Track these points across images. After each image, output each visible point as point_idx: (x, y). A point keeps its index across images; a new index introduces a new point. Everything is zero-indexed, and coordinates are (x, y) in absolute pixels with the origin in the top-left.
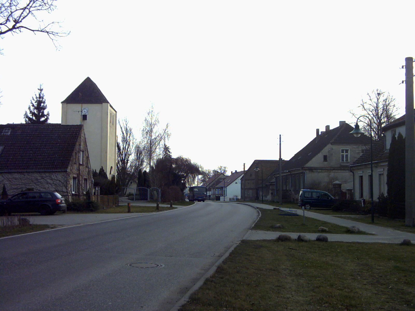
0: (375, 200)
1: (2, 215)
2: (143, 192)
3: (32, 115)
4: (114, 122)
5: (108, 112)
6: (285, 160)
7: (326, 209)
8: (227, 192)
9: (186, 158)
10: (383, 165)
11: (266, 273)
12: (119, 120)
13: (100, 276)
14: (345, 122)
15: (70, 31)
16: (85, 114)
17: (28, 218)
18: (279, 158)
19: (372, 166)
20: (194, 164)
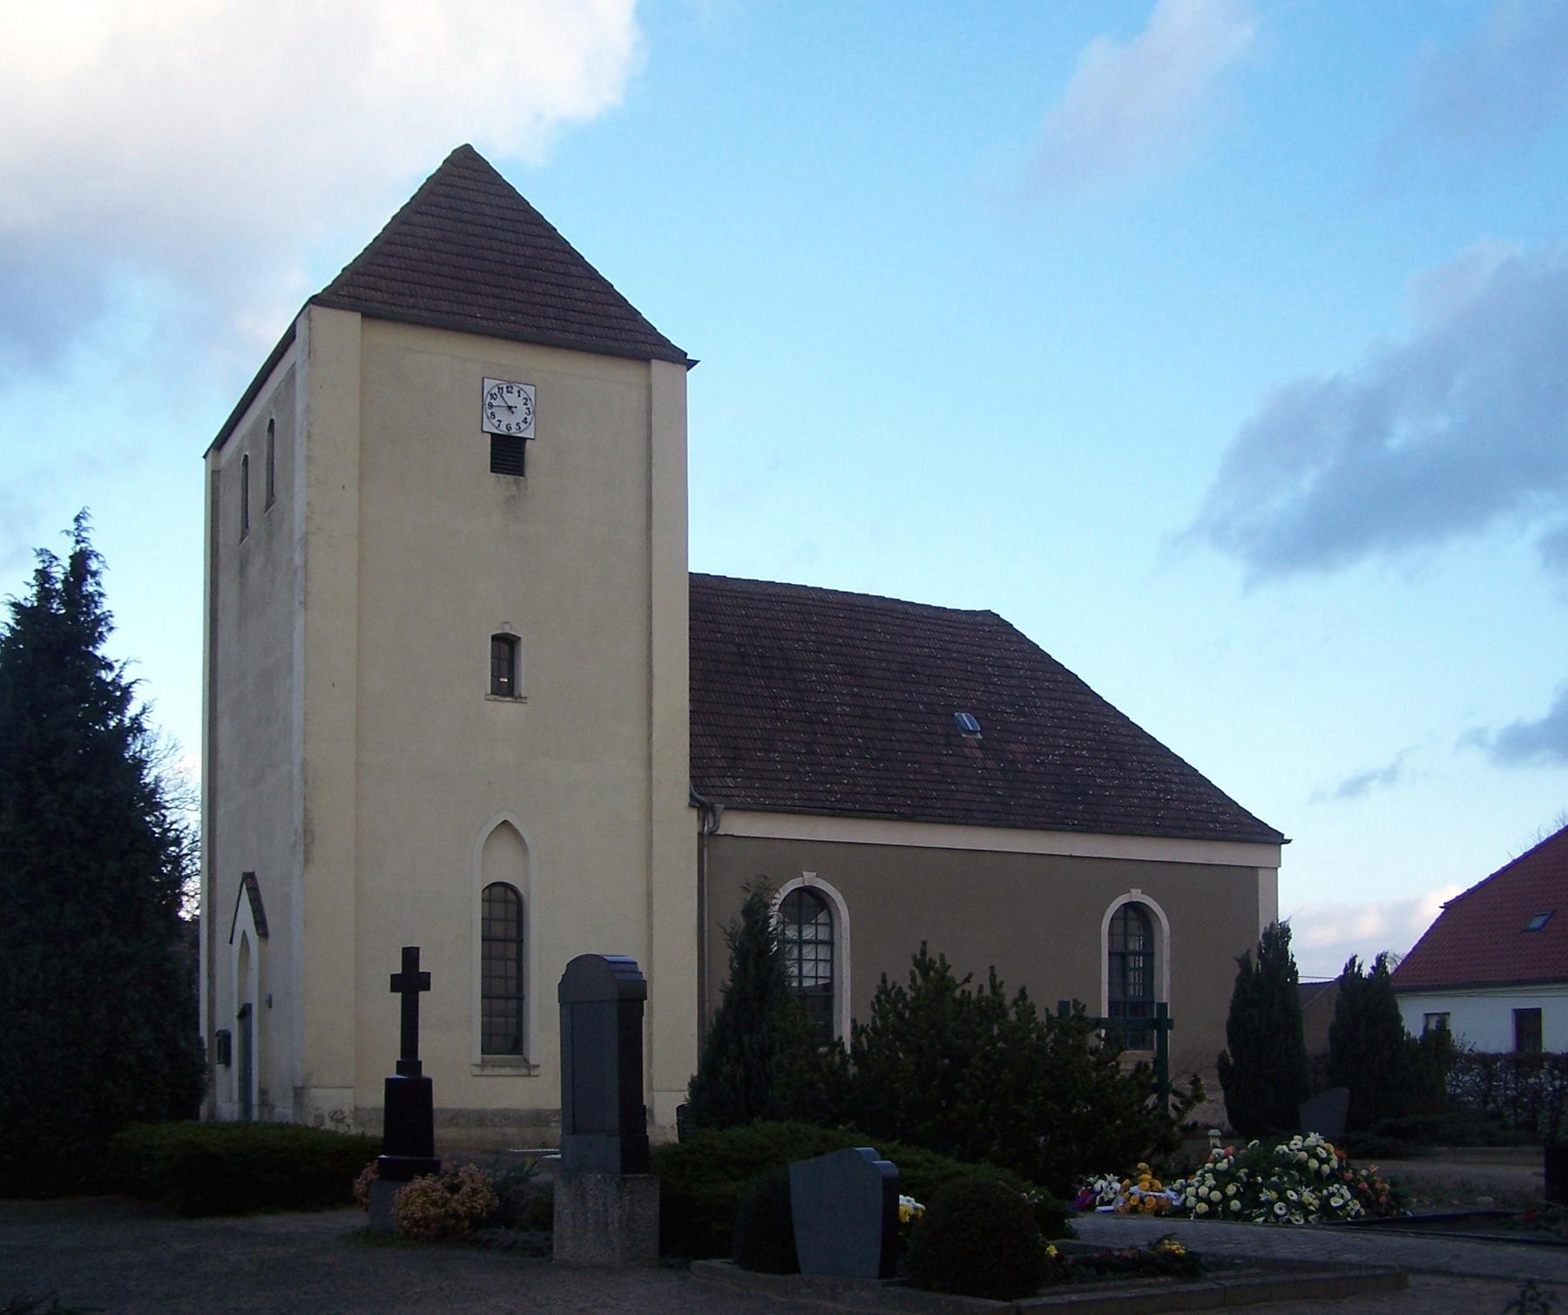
0: (94, 574)
1: (643, 16)
2: (491, 301)
3: (1015, 1003)
4: (222, 551)
5: (197, 937)
6: (693, 1070)
7: (1525, 1236)
8: (656, 1048)
9: (1132, 1247)
10: (210, 992)
11: (1014, 1009)
12: (263, 1092)
13: (51, 1007)
14: (428, 988)
15: (970, 975)
16: (514, 432)
17: (1308, 482)
18: (396, 1055)
19: (823, 942)
20: (608, 1003)
